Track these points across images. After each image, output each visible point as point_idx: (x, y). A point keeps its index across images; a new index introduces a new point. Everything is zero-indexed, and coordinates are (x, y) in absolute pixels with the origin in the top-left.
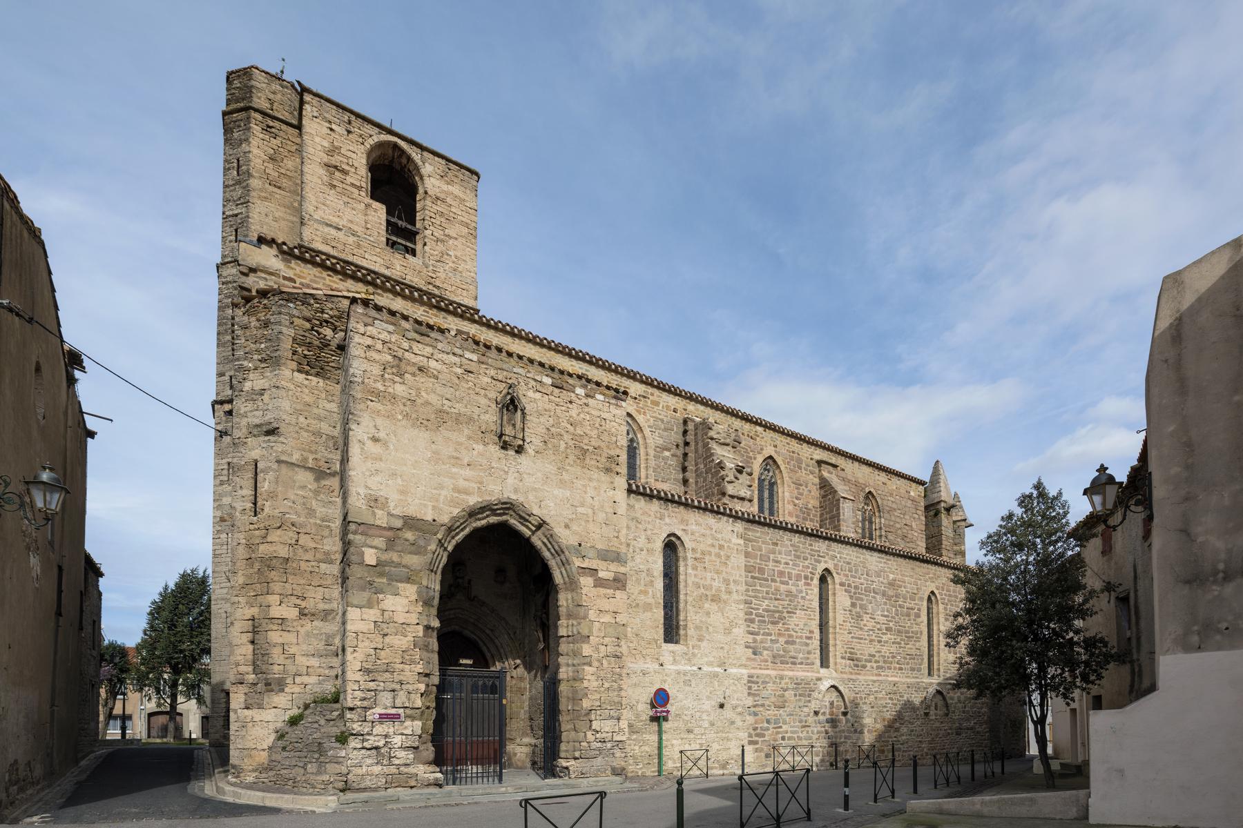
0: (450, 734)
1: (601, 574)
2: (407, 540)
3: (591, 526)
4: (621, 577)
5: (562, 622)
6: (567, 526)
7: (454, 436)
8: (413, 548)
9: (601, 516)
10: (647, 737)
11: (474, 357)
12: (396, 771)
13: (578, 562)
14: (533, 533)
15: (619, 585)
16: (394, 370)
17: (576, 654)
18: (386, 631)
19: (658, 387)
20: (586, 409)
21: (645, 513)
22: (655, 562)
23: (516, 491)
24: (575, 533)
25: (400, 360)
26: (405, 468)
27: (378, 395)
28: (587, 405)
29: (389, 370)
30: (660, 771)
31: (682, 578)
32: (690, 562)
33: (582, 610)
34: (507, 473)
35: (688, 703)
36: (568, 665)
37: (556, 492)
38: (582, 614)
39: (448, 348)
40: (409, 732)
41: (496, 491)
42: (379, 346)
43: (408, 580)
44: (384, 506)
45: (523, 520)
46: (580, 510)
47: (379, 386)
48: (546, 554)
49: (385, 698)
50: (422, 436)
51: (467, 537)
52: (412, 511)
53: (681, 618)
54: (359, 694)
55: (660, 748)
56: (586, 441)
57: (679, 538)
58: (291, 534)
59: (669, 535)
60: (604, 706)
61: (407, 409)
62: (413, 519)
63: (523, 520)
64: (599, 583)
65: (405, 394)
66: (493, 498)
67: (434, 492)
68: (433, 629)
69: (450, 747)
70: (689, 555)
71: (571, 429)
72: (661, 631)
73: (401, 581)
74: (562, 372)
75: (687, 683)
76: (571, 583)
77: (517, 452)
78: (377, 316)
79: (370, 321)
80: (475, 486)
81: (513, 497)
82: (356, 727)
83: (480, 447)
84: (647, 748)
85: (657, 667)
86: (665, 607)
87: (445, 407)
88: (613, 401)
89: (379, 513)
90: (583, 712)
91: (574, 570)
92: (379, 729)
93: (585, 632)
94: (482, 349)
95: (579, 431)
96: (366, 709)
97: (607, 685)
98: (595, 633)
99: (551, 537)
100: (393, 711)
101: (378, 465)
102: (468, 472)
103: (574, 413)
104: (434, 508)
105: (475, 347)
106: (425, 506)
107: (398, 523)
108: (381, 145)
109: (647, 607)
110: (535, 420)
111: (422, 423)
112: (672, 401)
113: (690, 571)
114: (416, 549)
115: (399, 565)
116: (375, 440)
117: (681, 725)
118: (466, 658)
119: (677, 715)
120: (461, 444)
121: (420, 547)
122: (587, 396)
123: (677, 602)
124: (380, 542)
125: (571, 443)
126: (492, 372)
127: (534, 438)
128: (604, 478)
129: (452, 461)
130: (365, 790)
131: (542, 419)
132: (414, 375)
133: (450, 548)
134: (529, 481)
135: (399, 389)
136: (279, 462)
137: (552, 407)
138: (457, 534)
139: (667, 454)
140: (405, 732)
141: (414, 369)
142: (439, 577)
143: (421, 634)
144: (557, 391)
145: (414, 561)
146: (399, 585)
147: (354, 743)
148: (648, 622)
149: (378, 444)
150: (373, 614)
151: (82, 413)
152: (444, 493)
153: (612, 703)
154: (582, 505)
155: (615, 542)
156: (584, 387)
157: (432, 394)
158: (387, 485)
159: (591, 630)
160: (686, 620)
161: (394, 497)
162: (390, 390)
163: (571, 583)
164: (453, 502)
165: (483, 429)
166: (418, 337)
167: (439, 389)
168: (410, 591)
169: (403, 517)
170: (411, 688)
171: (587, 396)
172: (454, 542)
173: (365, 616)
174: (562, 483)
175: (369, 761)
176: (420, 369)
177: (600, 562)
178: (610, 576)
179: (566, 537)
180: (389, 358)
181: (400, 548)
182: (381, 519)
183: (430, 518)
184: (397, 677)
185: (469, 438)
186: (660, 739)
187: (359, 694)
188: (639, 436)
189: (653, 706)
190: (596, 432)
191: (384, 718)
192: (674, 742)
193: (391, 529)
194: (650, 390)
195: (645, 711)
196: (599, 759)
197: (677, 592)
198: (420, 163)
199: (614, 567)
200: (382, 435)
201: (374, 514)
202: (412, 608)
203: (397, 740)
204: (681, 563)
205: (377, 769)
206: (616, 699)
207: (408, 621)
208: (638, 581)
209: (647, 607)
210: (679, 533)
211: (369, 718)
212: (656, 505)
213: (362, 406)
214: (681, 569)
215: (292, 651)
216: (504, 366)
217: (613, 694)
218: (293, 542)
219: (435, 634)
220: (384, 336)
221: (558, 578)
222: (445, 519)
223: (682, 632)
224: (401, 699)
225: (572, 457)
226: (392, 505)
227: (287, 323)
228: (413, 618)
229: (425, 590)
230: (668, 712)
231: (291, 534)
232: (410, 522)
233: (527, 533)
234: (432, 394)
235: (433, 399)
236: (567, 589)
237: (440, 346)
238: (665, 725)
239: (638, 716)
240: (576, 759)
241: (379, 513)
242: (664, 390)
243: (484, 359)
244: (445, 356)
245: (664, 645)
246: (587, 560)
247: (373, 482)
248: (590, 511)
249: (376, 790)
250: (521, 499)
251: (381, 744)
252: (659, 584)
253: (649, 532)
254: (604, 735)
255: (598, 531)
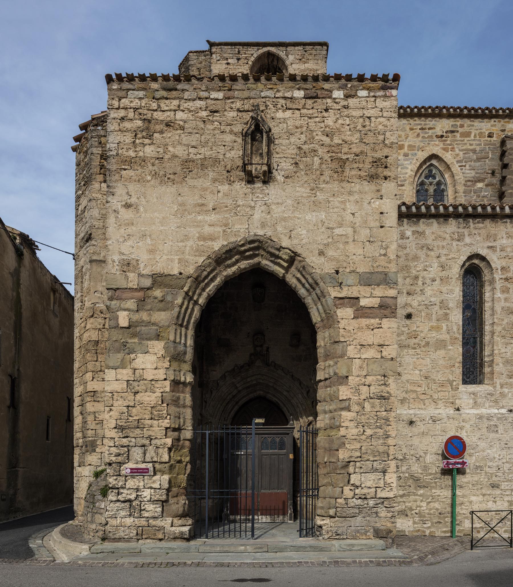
0: (244, 486)
1: (363, 302)
2: (156, 298)
3: (351, 248)
4: (390, 301)
5: (321, 365)
6: (321, 253)
7: (199, 183)
8: (161, 305)
9: (364, 233)
10: (438, 492)
11: (220, 95)
12: (145, 523)
13: (334, 293)
14: (287, 269)
15: (387, 312)
16: (144, 134)
17: (333, 398)
18: (137, 388)
19: (469, 116)
20: (346, 112)
21: (438, 237)
22: (452, 291)
23: (263, 225)
24: (332, 259)
25: (149, 121)
26: (153, 227)
27: (130, 162)
28: (346, 107)
29: (139, 136)
30: (452, 532)
31: (487, 306)
32: (498, 285)
33: (339, 348)
34: (253, 208)
35: (494, 452)
36: (325, 412)
37: (308, 217)
38: (339, 352)
39: (194, 95)
40: (157, 485)
41: (240, 231)
42: (131, 115)
43: (158, 337)
44: (136, 267)
45: (274, 257)
46: (337, 231)
47: (132, 154)
48: (302, 292)
49: (137, 453)
50: (170, 190)
51: (220, 290)
52: (159, 268)
53: (487, 352)
54: (114, 450)
55: (453, 505)
56: (345, 150)
57: (483, 259)
58: (100, 320)
59: (470, 258)
60: (366, 457)
61: (155, 168)
62: (161, 275)
63: (274, 257)
64: (361, 313)
65: (154, 154)
66: (239, 239)
67: (181, 244)
68: (184, 384)
69: (243, 500)
70: (497, 276)
71: (327, 140)
72: (458, 371)
73: (150, 339)
74: (316, 79)
75: (493, 429)
76: (328, 319)
77: (265, 182)
78: (130, 86)
79: (121, 94)
80: (220, 229)
81: (261, 232)
82: (112, 481)
83: (225, 188)
84: (436, 505)
85: (451, 411)
86: (465, 344)
87: (191, 156)
88: (381, 93)
89: (131, 275)
90: (340, 464)
91: (330, 302)
92: (131, 483)
93: (343, 372)
94: (228, 82)
95: (337, 140)
96: (120, 464)
97: (369, 432)
98: (355, 372)
99: (303, 270)
100: (143, 466)
101: (132, 230)
102: (213, 217)
103: (330, 122)
104: (180, 261)
105: (221, 84)
106: (172, 260)
107: (148, 283)
108: (259, 58)
109: (441, 344)
110: (285, 142)
111: (165, 179)
112: (485, 126)
113: (498, 294)
114: (164, 304)
115: (149, 323)
116: (128, 206)
117: (483, 478)
118: (259, 417)
119: (477, 467)
120: (205, 189)
121: (168, 302)
122: (347, 96)
123: (482, 335)
124: (131, 304)
125: (327, 157)
126: (238, 104)
127: (282, 165)
128: (368, 187)
129: (198, 209)
130: (119, 540)
131: (293, 139)
132: (161, 132)
133: (201, 301)
134: (277, 211)
135: (149, 151)
136: (91, 261)
137: (303, 122)
138: (207, 285)
139: (480, 185)
140: (154, 486)
141: (162, 127)
142: (191, 332)
143: (168, 389)
144: (310, 102)
145: (162, 317)
146: (149, 342)
147: (112, 496)
148: (441, 362)
149: (131, 209)
150: (125, 374)
151: (61, 284)
152: (190, 243)
153: (376, 453)
154: (340, 225)
155: (382, 261)
156: (343, 87)
157: (178, 146)
158: (138, 248)
159: (349, 370)
160: (492, 354)
161: (144, 257)
162: (141, 154)
163: (328, 319)
164: (198, 252)
165: (229, 168)
166: (164, 93)
167: (185, 139)
168: (158, 347)
169: (152, 276)
170: (158, 442)
171: (347, 96)
172: (205, 295)
173: (119, 377)
174: (316, 205)
175: (123, 513)
176: (167, 125)
177: (361, 288)
178: (375, 302)
179: (319, 265)
180: (139, 123)
181: (149, 307)
182: (133, 280)
183: (176, 272)
184: (146, 433)
185: (215, 180)
186: (454, 495)
187: (114, 450)
188: (446, 176)
189: (444, 457)
190: (358, 135)
191: (135, 472)
192: (473, 498)
193: (142, 289)
194: (459, 122)
195: (434, 462)
196: (359, 518)
197: (482, 324)
198: (284, 57)
199: (379, 291)
200: (133, 200)
201: (127, 278)
202: (160, 365)
203: (147, 494)
204: (487, 288)
205: (129, 521)
206: (381, 449)
207: (155, 378)
208: (429, 317)
209: (441, 344)
210: (483, 252)
211: (123, 472)
212: (452, 226)
213: (117, 177)
214: (487, 296)
215: (101, 418)
216: (252, 94)
217: (378, 443)
218: (101, 326)
219: (188, 389)
220: (136, 103)
221: (315, 317)
222: (191, 270)
223: (487, 370)
224: (151, 453)
225: (327, 173)
226: (142, 266)
227: (96, 144)
228: (161, 374)
229: (171, 345)
230: (464, 463)
231: (100, 320)
232: (159, 279)
233: (280, 271)
234: (178, 146)
235: (180, 151)
236: (324, 327)
237: (186, 95)
238: (460, 480)
239: (425, 468)
240: (331, 517)
241: (131, 275)
242: (476, 116)
243: (230, 93)
244: (191, 104)
245: (462, 388)
246: (345, 289)
247: (125, 248)
248: (350, 231)
249: (129, 540)
250: (269, 234)
251: (133, 497)
252: (457, 317)
253: (443, 259)
254: (365, 491)
255: (360, 251)
